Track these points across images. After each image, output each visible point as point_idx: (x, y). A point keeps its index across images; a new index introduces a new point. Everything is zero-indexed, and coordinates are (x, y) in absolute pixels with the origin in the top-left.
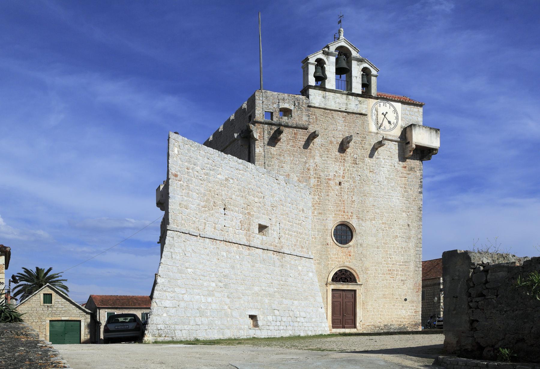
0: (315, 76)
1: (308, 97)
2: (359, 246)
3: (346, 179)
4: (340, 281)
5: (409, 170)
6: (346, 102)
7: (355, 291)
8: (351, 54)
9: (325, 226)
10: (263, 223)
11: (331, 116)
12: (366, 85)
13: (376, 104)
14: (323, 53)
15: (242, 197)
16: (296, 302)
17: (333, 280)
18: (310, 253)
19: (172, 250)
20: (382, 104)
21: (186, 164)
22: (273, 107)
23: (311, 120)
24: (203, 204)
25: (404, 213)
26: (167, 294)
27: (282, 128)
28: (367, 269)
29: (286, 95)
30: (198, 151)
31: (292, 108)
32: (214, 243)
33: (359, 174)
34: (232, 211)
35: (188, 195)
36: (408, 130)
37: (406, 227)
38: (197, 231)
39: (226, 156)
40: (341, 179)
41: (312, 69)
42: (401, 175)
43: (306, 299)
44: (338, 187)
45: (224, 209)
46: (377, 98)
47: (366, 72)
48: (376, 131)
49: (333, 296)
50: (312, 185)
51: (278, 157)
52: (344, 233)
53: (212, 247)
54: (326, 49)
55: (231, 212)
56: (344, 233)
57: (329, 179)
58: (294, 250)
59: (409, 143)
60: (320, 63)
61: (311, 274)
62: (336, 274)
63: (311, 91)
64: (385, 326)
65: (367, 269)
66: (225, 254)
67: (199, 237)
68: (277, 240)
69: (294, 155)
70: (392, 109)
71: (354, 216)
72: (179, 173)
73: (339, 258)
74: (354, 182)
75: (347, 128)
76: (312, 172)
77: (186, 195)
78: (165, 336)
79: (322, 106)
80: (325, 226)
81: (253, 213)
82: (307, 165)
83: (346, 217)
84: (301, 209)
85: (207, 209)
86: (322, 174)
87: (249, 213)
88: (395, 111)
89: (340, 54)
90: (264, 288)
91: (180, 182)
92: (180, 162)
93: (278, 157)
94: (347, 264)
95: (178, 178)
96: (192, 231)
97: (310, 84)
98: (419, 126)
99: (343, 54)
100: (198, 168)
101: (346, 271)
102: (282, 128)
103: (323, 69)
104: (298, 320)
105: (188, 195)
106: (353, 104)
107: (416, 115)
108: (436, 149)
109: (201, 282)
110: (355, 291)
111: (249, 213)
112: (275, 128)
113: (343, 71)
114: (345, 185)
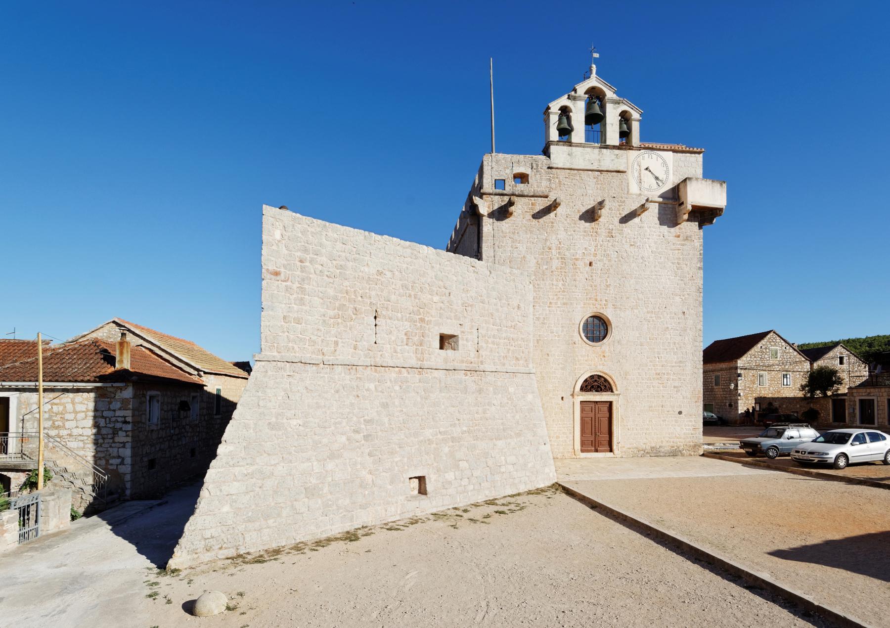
0: (559, 130)
1: (549, 157)
2: (616, 344)
3: (599, 257)
4: (590, 390)
5: (685, 240)
6: (598, 157)
7: (611, 403)
8: (604, 95)
9: (570, 320)
10: (447, 331)
11: (578, 178)
12: (625, 135)
13: (638, 156)
14: (569, 98)
15: (410, 296)
16: (500, 443)
17: (582, 389)
18: (531, 366)
19: (260, 394)
20: (646, 156)
21: (299, 254)
22: (507, 174)
23: (553, 186)
24: (331, 313)
25: (677, 298)
26: (237, 469)
27: (514, 198)
28: (626, 374)
29: (522, 156)
30: (324, 233)
31: (528, 171)
32: (353, 372)
33: (617, 249)
34: (390, 318)
35: (301, 302)
36: (681, 187)
37: (681, 315)
38: (320, 357)
39: (378, 237)
40: (592, 259)
41: (554, 119)
42: (673, 247)
43: (519, 435)
44: (588, 268)
45: (375, 318)
46: (639, 148)
47: (625, 118)
48: (638, 192)
49: (582, 410)
50: (554, 268)
51: (512, 236)
52: (598, 328)
53: (348, 377)
54: (573, 93)
55: (389, 321)
56: (598, 328)
57: (577, 259)
58: (504, 365)
59: (683, 203)
60: (565, 111)
61: (530, 397)
62: (586, 381)
63: (553, 149)
64: (652, 448)
65: (626, 374)
66: (372, 386)
67: (322, 365)
68: (473, 354)
69: (531, 232)
70: (660, 161)
71: (610, 305)
72: (282, 270)
73: (592, 359)
74: (610, 261)
75: (599, 192)
76: (554, 251)
77: (297, 302)
78: (221, 548)
79: (568, 166)
80: (570, 320)
81: (430, 318)
82: (548, 243)
83: (599, 307)
84: (516, 305)
85: (340, 320)
86: (567, 253)
87: (422, 320)
88: (665, 163)
89: (591, 98)
90: (442, 430)
91: (285, 283)
92: (285, 251)
93: (512, 236)
94: (600, 368)
95: (282, 277)
96: (307, 357)
97: (551, 139)
98: (697, 179)
99: (595, 95)
100: (324, 259)
101: (599, 377)
102: (514, 198)
103: (569, 119)
104: (503, 469)
105: (301, 302)
106: (609, 159)
107: (694, 164)
108: (721, 210)
109: (316, 438)
110: (611, 403)
111: (422, 320)
112: (506, 199)
113: (595, 119)
114: (597, 265)
